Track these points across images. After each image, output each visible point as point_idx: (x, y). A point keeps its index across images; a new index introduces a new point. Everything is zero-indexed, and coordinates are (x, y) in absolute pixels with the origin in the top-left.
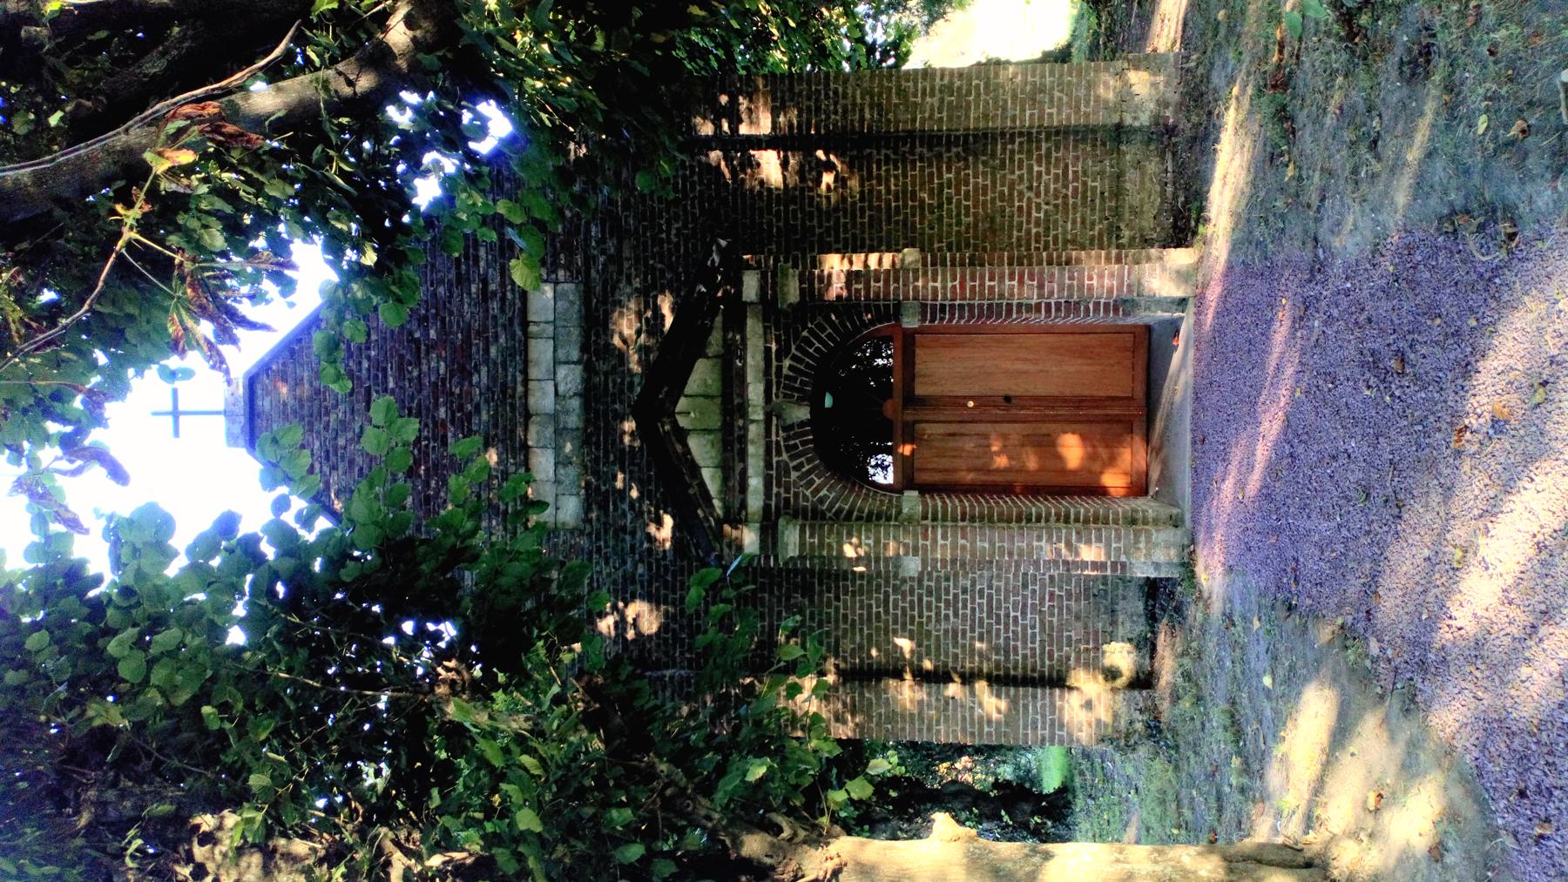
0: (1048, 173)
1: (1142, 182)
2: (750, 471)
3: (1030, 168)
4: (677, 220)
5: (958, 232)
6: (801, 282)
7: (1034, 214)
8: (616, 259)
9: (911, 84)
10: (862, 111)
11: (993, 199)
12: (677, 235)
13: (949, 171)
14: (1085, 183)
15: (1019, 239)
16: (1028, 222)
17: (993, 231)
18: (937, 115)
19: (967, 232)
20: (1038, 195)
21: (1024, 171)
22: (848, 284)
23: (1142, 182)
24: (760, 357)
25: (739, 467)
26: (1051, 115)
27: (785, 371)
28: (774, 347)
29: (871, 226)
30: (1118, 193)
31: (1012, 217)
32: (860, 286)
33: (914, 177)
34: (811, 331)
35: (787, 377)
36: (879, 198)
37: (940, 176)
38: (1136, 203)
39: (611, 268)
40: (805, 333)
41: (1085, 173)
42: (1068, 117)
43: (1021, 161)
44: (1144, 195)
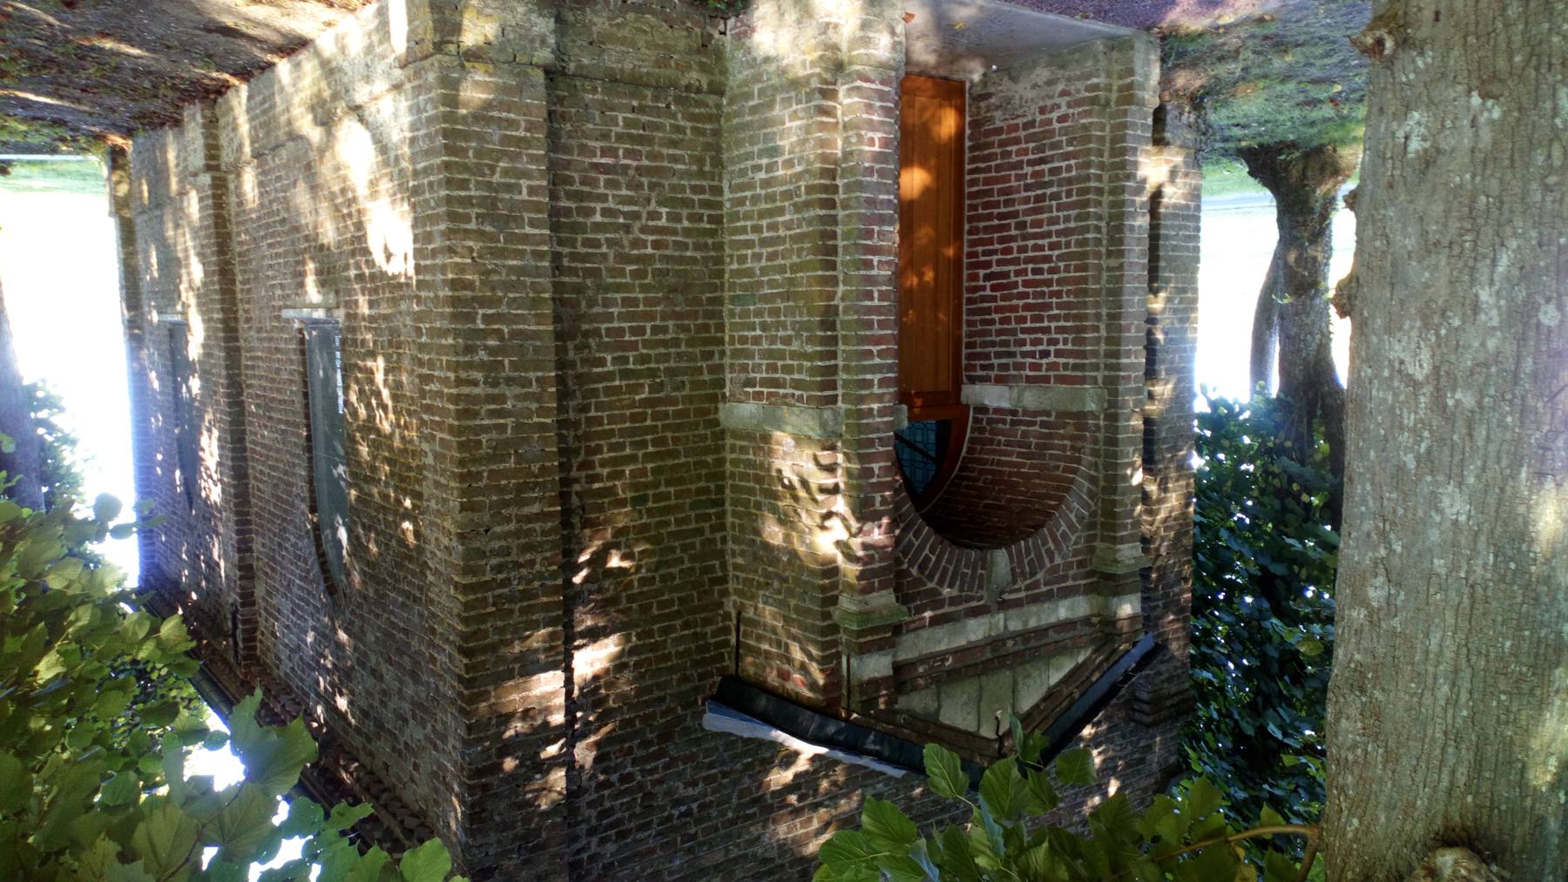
0: (604, 198)
1: (623, 41)
2: (1053, 620)
3: (598, 227)
5: (690, 343)
7: (663, 222)
9: (484, 438)
10: (530, 519)
11: (644, 288)
12: (695, 784)
13: (602, 362)
14: (620, 137)
15: (697, 247)
16: (674, 232)
17: (687, 287)
18: (534, 388)
19: (686, 329)
20: (636, 216)
21: (601, 237)
22: (875, 517)
23: (623, 41)
24: (940, 631)
25: (1053, 636)
26: (532, 191)
27: (955, 592)
28: (928, 614)
29: (681, 481)
30: (635, 83)
33: (612, 420)
34: (911, 564)
35: (961, 590)
36: (643, 472)
37: (610, 376)
38: (651, 55)
40: (914, 571)
41: (605, 136)
42: (534, 159)
43: (588, 243)
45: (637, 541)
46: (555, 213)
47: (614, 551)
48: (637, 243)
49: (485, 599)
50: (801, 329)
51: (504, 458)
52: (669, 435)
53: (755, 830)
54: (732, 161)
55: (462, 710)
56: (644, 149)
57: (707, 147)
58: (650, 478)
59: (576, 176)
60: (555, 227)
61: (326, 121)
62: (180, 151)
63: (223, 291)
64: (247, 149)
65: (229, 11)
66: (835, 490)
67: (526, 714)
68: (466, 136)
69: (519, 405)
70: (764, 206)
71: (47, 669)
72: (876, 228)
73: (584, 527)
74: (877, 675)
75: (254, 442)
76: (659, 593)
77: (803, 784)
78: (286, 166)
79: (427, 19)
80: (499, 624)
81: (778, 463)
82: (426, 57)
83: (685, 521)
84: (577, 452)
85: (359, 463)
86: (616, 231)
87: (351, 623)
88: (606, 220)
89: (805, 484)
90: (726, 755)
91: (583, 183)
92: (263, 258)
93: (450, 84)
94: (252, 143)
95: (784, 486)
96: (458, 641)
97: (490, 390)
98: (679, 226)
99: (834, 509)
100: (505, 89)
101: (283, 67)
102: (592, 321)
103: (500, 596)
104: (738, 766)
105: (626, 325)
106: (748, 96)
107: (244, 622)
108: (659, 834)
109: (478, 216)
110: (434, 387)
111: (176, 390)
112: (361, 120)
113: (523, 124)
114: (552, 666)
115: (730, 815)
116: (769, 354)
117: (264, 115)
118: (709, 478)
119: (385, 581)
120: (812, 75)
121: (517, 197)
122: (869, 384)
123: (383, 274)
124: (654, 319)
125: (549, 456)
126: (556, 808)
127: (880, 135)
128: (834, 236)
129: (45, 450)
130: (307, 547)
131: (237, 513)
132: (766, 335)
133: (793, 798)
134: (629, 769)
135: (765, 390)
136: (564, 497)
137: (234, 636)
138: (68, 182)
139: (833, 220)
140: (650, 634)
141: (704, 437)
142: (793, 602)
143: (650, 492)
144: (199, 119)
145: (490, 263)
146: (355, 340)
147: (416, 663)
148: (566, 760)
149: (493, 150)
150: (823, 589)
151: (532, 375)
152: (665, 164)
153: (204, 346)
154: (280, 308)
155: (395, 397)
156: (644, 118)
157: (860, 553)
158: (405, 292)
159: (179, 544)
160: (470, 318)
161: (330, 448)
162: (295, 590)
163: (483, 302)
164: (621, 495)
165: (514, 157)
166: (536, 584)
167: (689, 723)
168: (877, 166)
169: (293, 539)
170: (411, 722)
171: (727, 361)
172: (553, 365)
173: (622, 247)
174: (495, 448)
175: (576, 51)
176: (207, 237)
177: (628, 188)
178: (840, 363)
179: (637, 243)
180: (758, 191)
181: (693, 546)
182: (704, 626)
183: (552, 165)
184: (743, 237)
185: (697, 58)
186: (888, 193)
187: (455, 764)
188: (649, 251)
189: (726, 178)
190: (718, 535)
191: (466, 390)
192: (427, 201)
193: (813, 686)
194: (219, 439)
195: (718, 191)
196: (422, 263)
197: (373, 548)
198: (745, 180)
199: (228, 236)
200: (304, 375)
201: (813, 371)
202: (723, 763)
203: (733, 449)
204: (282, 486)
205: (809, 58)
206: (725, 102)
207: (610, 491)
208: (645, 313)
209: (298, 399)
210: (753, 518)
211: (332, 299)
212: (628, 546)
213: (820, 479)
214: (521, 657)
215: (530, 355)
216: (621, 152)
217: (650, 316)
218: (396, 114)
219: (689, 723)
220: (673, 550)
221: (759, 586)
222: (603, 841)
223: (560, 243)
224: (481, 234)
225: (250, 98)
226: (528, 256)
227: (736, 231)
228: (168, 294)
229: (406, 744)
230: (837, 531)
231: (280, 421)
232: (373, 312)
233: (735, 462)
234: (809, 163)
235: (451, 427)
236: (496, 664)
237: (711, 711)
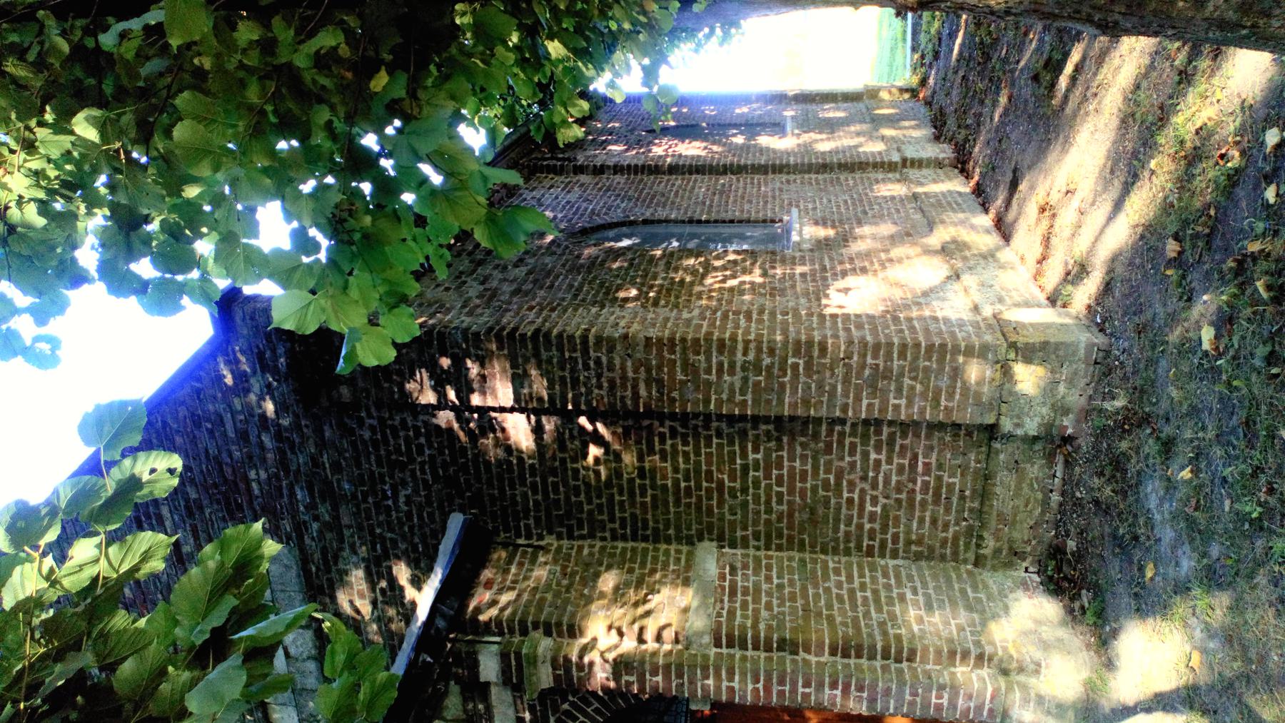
0: (889, 461)
3: (866, 455)
4: (404, 484)
5: (768, 522)
6: (554, 668)
7: (869, 508)
8: (335, 525)
9: (702, 358)
11: (814, 489)
12: (408, 503)
13: (756, 450)
14: (939, 478)
15: (847, 534)
16: (861, 516)
17: (813, 521)
18: (738, 398)
19: (780, 520)
20: (874, 486)
21: (858, 457)
22: (616, 675)
26: (897, 407)
29: (655, 507)
30: (984, 495)
31: (838, 509)
32: (633, 679)
33: (709, 455)
34: (572, 704)
36: (664, 477)
37: (744, 455)
38: (1008, 509)
39: (329, 536)
40: (566, 706)
41: (940, 467)
44: (1019, 502)
45: (609, 469)
46: (878, 423)
47: (602, 451)
48: (852, 485)
49: (575, 351)
50: (779, 620)
51: (684, 371)
52: (694, 500)
53: (363, 551)
54: (920, 569)
55: (491, 329)
56: (929, 498)
57: (931, 549)
58: (659, 483)
59: (907, 442)
60: (866, 422)
61: (945, 251)
62: (916, 137)
63: (810, 165)
64: (920, 190)
65: (1032, 188)
66: (641, 641)
67: (483, 378)
68: (941, 360)
69: (726, 386)
70: (883, 594)
71: (555, 48)
72: (865, 695)
73: (623, 427)
74: (481, 668)
75: (696, 181)
76: (566, 484)
77: (394, 594)
78: (907, 216)
79: (1035, 338)
80: (555, 360)
81: (666, 592)
82: (1004, 335)
83: (622, 510)
84: (685, 426)
85: (680, 258)
86: (862, 469)
87: (559, 246)
88: (871, 462)
89: (648, 614)
90: (427, 530)
91: (902, 446)
92: (836, 196)
93: (983, 352)
94: (925, 193)
95: (646, 595)
96: (544, 329)
97: (739, 365)
98: (865, 520)
99: (625, 638)
100: (978, 395)
101: (986, 220)
102: (789, 444)
103: (576, 362)
104: (417, 540)
105: (785, 471)
106: (975, 588)
107: (562, 166)
108: (372, 473)
109: (877, 365)
110: (743, 322)
111: (735, 126)
112: (949, 278)
113: (951, 404)
114: (517, 398)
115: (378, 531)
116: (757, 590)
117: (946, 203)
118: (656, 530)
119: (590, 273)
120: (996, 648)
121: (892, 395)
122: (731, 679)
123: (827, 287)
124: (789, 494)
125: (684, 405)
126: (406, 395)
127: (945, 704)
128: (859, 656)
129: (691, 32)
130: (617, 215)
131: (643, 166)
132: (775, 586)
133: (384, 584)
134: (427, 452)
135: (727, 584)
136: (649, 413)
137: (552, 158)
138: (887, 54)
139: (872, 657)
140: (533, 474)
141: (689, 529)
142: (549, 596)
143: (647, 482)
144: (942, 156)
145: (840, 371)
146: (775, 261)
147: (526, 293)
148: (443, 404)
149: (929, 380)
150: (559, 624)
151: (749, 397)
152: (917, 514)
153: (768, 149)
154: (797, 206)
155: (731, 289)
156: (955, 500)
157: (586, 660)
158: (815, 304)
159: (619, 120)
160: (797, 353)
161: (693, 236)
162: (585, 205)
163: (808, 365)
164: (647, 459)
165: (924, 395)
166: (583, 390)
167: (458, 501)
168: (918, 699)
169: (623, 205)
170: (482, 288)
171: (752, 552)
172: (756, 413)
173: (849, 473)
174: (693, 365)
175: (1010, 450)
176: (852, 156)
177: (898, 482)
178: (750, 653)
179: (852, 485)
180: (895, 591)
181: (601, 512)
182: (535, 518)
183: (916, 424)
184: (856, 574)
185: (1006, 546)
186: (896, 708)
187: (450, 321)
188: (845, 495)
189: (906, 563)
190: (607, 534)
191: (740, 347)
192: (888, 327)
193: (478, 610)
194: (699, 157)
195: (895, 555)
196: (839, 320)
197: (615, 266)
198: (904, 579)
199: (853, 171)
200: (749, 221)
201: (743, 627)
202: (421, 527)
203: (678, 552)
204: (663, 200)
205: (1010, 646)
206: (969, 567)
207: (651, 451)
208: (794, 488)
209: (729, 216)
210: (621, 566)
211: (806, 246)
212: (606, 461)
213: (652, 626)
214: (526, 374)
215: (765, 396)
216: (927, 478)
217: (791, 491)
218: (955, 307)
219: (458, 501)
220: (599, 497)
221: (564, 568)
222: (372, 428)
223: (854, 425)
224: (863, 366)
225: (960, 194)
226: (844, 400)
227: (861, 568)
228: (806, 124)
229: (465, 282)
230: (606, 640)
231: (712, 201)
232: (797, 277)
233: (667, 552)
234: (921, 638)
235: (712, 333)
236: (523, 356)
237: (465, 520)
